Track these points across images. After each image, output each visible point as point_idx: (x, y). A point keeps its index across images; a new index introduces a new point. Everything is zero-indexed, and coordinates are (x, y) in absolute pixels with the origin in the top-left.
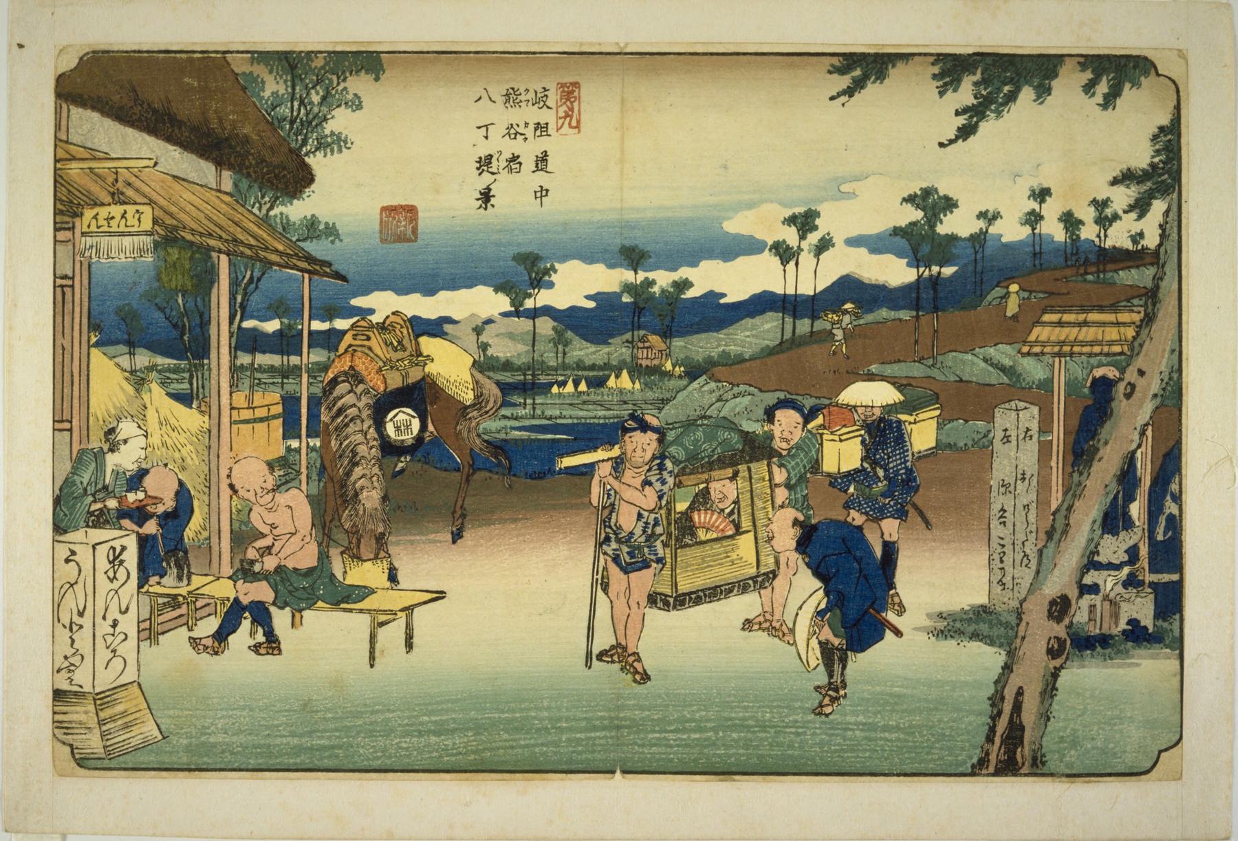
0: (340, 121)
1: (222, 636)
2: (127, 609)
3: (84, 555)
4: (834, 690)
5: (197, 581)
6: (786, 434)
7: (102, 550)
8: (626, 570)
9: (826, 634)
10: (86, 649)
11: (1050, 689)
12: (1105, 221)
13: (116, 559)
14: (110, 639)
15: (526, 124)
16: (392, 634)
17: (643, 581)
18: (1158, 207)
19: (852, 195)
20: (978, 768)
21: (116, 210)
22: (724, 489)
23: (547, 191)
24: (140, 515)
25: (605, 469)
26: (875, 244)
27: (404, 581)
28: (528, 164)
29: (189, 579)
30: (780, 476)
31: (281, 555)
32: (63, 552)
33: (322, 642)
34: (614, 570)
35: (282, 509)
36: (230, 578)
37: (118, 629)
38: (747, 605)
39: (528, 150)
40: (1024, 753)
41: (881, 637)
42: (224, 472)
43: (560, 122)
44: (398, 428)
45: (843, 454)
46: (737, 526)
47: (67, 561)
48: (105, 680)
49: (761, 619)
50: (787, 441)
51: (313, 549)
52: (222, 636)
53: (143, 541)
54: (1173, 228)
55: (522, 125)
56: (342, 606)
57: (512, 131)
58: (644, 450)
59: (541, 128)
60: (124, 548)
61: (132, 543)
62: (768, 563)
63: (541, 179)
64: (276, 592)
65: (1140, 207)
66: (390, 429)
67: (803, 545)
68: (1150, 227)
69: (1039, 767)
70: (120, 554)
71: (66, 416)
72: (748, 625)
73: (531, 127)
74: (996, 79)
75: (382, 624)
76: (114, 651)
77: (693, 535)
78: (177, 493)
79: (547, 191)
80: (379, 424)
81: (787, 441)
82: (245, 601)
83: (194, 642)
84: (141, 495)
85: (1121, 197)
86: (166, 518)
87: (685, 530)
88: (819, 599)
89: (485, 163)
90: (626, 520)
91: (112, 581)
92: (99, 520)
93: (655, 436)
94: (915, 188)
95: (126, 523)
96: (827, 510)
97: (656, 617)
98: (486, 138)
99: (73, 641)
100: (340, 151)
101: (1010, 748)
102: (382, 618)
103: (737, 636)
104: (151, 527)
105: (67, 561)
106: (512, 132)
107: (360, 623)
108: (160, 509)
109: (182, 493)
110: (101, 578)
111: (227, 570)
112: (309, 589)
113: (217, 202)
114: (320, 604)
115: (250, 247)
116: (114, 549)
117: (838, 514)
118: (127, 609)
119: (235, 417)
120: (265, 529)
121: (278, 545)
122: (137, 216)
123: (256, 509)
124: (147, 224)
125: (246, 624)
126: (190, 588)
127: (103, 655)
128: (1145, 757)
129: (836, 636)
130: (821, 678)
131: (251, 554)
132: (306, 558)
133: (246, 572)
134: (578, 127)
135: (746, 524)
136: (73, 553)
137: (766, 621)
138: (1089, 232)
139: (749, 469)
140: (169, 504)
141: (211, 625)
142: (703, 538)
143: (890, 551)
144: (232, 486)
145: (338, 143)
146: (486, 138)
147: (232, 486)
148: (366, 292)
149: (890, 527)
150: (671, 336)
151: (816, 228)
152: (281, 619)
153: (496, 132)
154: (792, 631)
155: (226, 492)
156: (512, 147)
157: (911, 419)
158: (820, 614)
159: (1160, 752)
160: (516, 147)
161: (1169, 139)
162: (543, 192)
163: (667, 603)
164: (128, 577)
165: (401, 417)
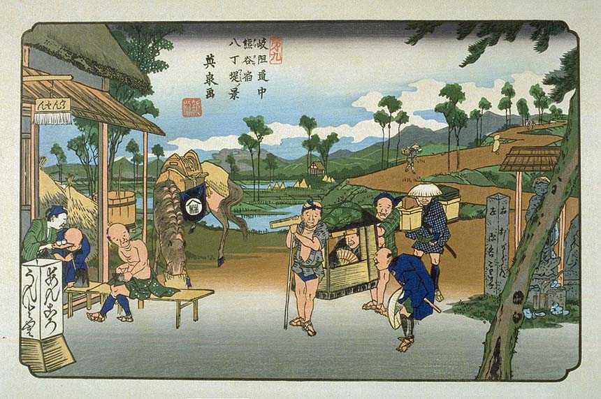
0: (163, 55)
1: (104, 312)
2: (57, 299)
3: (36, 271)
4: (410, 338)
5: (92, 285)
6: (384, 212)
7: (45, 270)
8: (305, 279)
9: (404, 311)
10: (36, 318)
11: (515, 336)
12: (541, 104)
13: (51, 275)
14: (47, 313)
15: (255, 56)
16: (188, 311)
17: (313, 285)
18: (569, 95)
19: (415, 89)
20: (477, 379)
21: (53, 101)
22: (352, 237)
23: (265, 90)
24: (64, 252)
25: (294, 229)
26: (425, 115)
27: (195, 285)
28: (255, 77)
29: (88, 284)
30: (381, 232)
31: (134, 272)
32: (25, 270)
33: (154, 313)
34: (298, 279)
35: (133, 249)
36: (107, 283)
37: (52, 309)
38: (364, 297)
39: (256, 69)
40: (503, 369)
41: (431, 313)
42: (105, 232)
43: (272, 57)
44: (191, 209)
45: (412, 221)
46: (359, 257)
47: (27, 275)
48: (46, 334)
49: (371, 304)
50: (384, 215)
51: (148, 270)
52: (104, 312)
53: (65, 264)
54: (576, 103)
55: (252, 57)
56: (163, 298)
57: (248, 60)
58: (313, 219)
59: (262, 58)
60: (55, 269)
61: (59, 266)
62: (374, 277)
63: (262, 83)
64: (131, 291)
65: (558, 97)
66: (188, 209)
67: (392, 267)
68: (564, 106)
69: (509, 378)
70: (53, 272)
71: (110, 209)
72: (365, 307)
73: (257, 57)
74: (487, 33)
75: (184, 306)
76: (50, 319)
77: (338, 262)
78: (82, 242)
79: (265, 90)
80: (183, 208)
81: (384, 215)
82: (114, 295)
83: (90, 316)
84: (64, 242)
85: (548, 90)
86: (76, 253)
87: (333, 259)
88: (399, 294)
89: (234, 76)
90: (305, 254)
91: (49, 285)
92: (45, 254)
93: (320, 211)
94: (443, 85)
95: (57, 256)
96: (406, 247)
97: (320, 302)
98: (235, 63)
99: (30, 314)
100: (158, 72)
101: (496, 367)
102: (182, 303)
103: (363, 310)
104: (69, 258)
105: (27, 275)
106: (248, 60)
107: (173, 306)
108: (74, 249)
109: (84, 241)
110: (43, 281)
111: (106, 280)
112: (141, 289)
113: (86, 90)
114: (152, 296)
115: (93, 113)
116: (49, 269)
117: (410, 252)
118: (57, 299)
119: (111, 203)
120: (124, 259)
121: (131, 268)
122: (62, 104)
123: (120, 249)
124: (68, 108)
125: (116, 307)
126: (89, 288)
127: (45, 321)
128: (559, 370)
129: (408, 312)
130: (401, 333)
131: (118, 271)
132: (145, 274)
133: (115, 280)
134: (281, 59)
135: (364, 257)
136: (30, 271)
137: (374, 305)
138: (533, 111)
139: (365, 229)
140: (77, 247)
141: (98, 307)
142: (342, 264)
143: (435, 270)
144: (109, 238)
145: (161, 66)
146: (235, 63)
147: (109, 238)
148: (174, 138)
149: (435, 257)
150: (256, 142)
151: (400, 108)
152: (133, 304)
153: (240, 60)
154: (387, 310)
155: (106, 240)
156: (246, 68)
157: (446, 203)
158: (400, 301)
159: (568, 371)
160: (250, 68)
161: (572, 62)
162: (262, 91)
163: (324, 296)
164: (57, 284)
165: (193, 203)
